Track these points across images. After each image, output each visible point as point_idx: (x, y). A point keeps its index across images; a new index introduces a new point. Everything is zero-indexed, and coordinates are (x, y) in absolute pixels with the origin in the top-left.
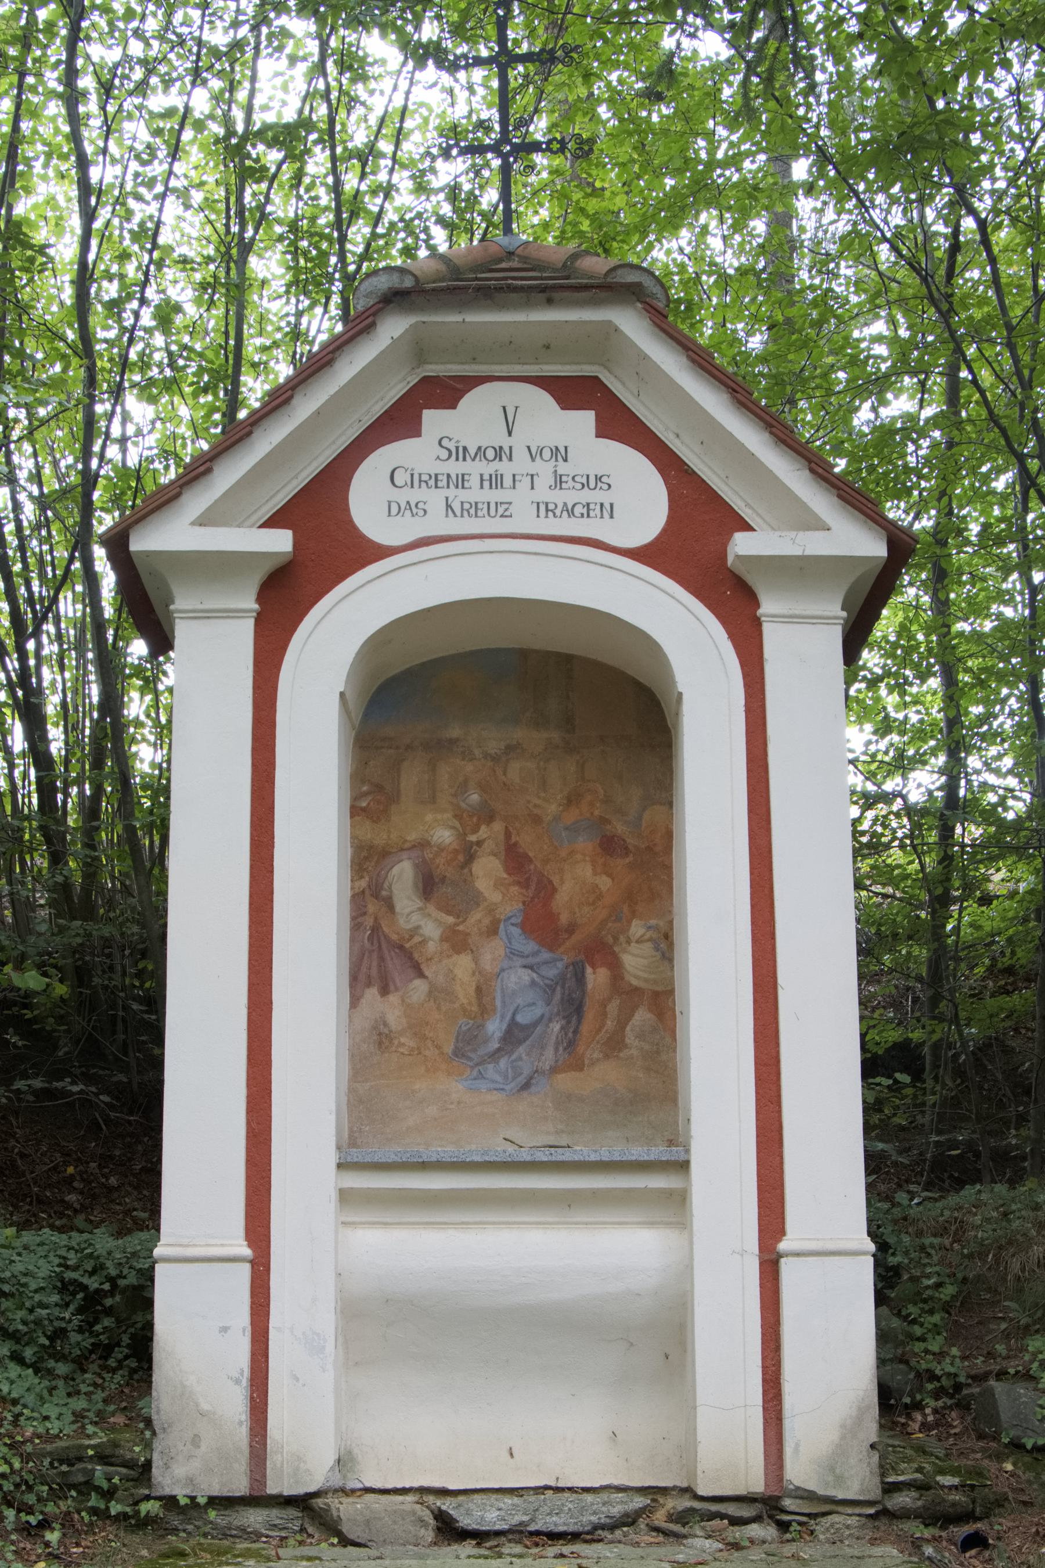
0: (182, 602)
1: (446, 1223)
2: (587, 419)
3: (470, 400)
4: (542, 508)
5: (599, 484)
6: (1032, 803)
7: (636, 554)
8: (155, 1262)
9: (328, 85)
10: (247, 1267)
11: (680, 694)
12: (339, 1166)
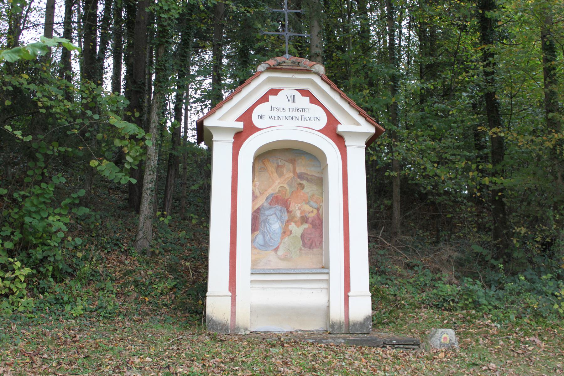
2: (308, 99)
7: (320, 131)
11: (327, 165)
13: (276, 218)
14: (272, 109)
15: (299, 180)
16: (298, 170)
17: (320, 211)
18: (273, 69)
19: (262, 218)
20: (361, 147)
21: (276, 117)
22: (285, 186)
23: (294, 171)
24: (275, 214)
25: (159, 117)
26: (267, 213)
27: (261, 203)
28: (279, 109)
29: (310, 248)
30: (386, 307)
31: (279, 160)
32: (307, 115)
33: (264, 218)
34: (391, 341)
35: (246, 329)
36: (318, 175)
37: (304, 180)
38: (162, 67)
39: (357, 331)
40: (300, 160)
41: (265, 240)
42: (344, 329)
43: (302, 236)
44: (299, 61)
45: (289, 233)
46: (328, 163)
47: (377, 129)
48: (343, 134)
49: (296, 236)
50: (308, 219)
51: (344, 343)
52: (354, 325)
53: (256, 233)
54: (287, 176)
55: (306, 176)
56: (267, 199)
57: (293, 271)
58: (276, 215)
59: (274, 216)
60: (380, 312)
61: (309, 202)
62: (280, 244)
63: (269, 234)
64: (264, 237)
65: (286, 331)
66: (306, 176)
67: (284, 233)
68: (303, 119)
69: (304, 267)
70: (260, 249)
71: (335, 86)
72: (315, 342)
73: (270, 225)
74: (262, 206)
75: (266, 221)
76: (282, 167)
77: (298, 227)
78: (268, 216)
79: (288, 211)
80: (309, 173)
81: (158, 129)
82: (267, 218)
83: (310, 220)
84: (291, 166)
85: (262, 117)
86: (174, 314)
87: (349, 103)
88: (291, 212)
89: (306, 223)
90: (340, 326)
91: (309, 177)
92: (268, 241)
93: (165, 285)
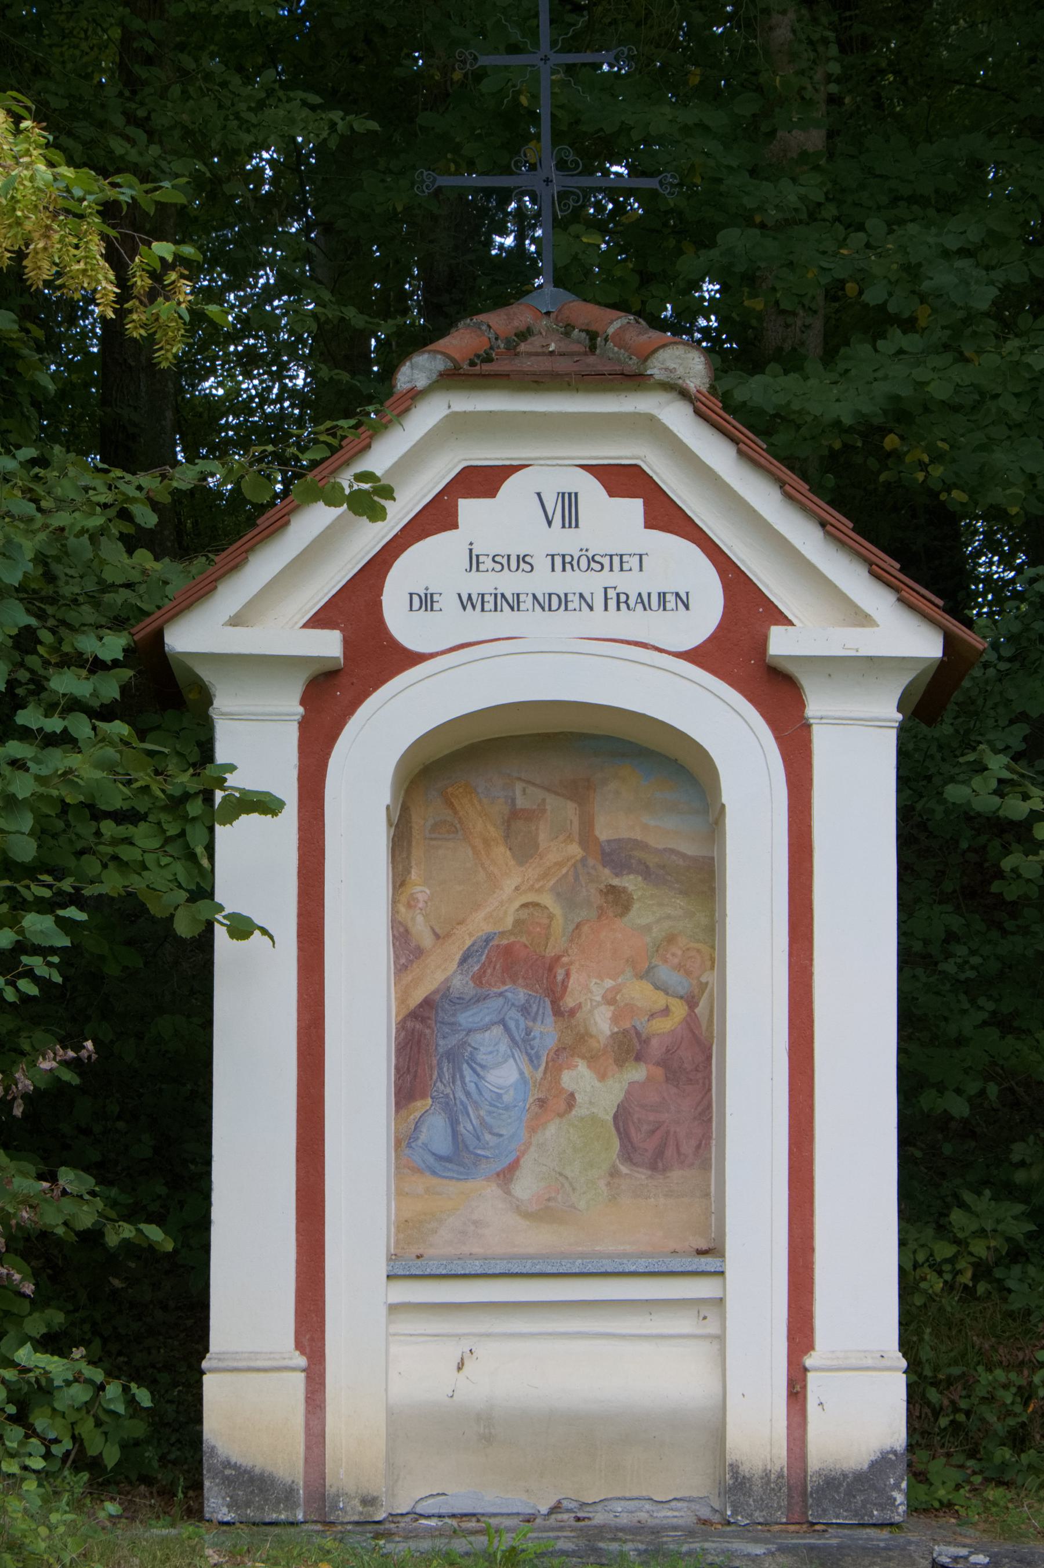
0: (223, 703)
1: (488, 1335)
2: (635, 507)
3: (510, 486)
4: (558, 561)
7: (691, 656)
10: (302, 1376)
11: (723, 806)
12: (388, 1276)
13: (506, 1040)
14: (474, 561)
15: (607, 871)
16: (604, 833)
17: (701, 1009)
22: (547, 900)
23: (587, 838)
24: (503, 1022)
28: (503, 562)
29: (653, 1167)
32: (630, 583)
33: (453, 1041)
36: (690, 849)
37: (631, 870)
43: (622, 1118)
45: (563, 1106)
46: (725, 799)
47: (950, 642)
48: (792, 669)
49: (593, 1118)
50: (646, 1042)
56: (464, 960)
59: (497, 1031)
61: (651, 969)
63: (477, 1106)
67: (542, 1103)
69: (628, 1248)
70: (434, 1173)
73: (479, 1069)
76: (529, 816)
77: (602, 1077)
79: (558, 1012)
80: (655, 841)
82: (464, 1044)
84: (570, 810)
85: (427, 601)
88: (572, 1013)
89: (638, 1058)
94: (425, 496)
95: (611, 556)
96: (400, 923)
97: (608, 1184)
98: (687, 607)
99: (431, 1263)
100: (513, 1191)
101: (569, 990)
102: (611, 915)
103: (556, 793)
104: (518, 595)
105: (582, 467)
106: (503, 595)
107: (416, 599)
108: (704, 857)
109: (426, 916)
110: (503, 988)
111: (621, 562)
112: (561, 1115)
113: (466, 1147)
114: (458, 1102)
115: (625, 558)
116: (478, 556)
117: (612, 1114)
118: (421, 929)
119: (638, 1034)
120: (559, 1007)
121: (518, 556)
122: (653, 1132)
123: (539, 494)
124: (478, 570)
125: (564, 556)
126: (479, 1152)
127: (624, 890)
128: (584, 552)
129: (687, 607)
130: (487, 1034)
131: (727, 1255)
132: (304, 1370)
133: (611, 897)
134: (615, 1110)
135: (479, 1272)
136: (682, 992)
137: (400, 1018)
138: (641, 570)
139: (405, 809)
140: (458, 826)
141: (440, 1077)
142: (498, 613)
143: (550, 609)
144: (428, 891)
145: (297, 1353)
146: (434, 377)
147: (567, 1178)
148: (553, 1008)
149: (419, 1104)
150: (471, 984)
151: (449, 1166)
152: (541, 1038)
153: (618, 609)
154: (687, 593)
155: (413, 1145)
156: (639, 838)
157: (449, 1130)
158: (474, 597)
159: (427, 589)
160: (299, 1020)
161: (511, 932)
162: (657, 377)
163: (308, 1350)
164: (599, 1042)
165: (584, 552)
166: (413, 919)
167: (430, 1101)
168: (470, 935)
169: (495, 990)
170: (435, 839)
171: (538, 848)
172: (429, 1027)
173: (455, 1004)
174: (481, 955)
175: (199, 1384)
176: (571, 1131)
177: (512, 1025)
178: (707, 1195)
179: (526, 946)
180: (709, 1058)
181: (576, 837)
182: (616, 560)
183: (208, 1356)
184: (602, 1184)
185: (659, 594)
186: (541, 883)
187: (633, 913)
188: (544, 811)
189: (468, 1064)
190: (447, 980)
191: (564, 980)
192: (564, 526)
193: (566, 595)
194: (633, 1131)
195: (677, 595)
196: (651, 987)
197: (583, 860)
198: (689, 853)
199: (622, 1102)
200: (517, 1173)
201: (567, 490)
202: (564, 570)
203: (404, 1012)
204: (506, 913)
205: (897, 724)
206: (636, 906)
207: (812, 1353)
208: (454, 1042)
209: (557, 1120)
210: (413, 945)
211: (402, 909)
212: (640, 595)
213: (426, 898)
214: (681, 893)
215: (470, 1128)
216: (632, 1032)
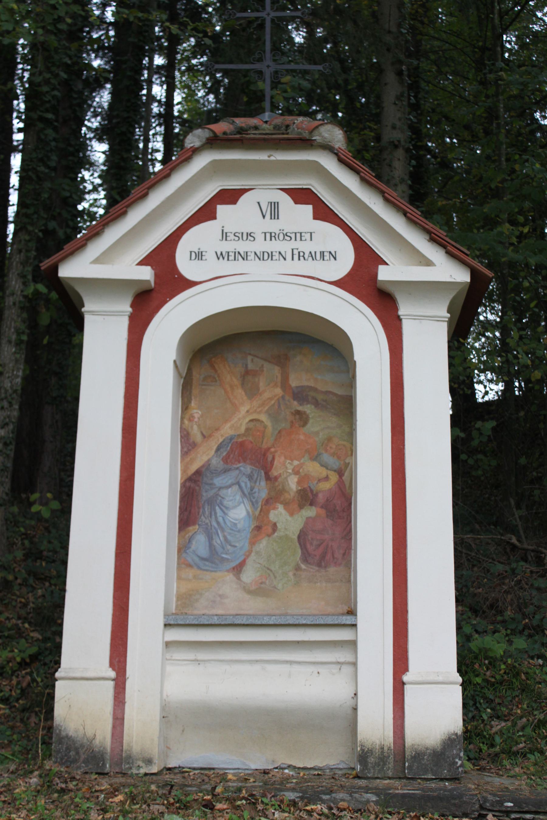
2: (308, 209)
3: (244, 199)
4: (268, 236)
5: (249, 238)
6: (495, 401)
7: (338, 283)
8: (56, 680)
9: (533, 551)
10: (112, 684)
11: (355, 362)
12: (165, 625)
13: (240, 493)
14: (225, 236)
15: (295, 403)
16: (294, 382)
17: (346, 477)
18: (222, 140)
19: (206, 495)
20: (436, 319)
21: (232, 254)
22: (263, 417)
23: (285, 384)
24: (238, 483)
25: (24, 284)
26: (218, 481)
27: (205, 458)
28: (239, 236)
29: (319, 565)
30: (530, 713)
31: (250, 358)
32: (306, 247)
33: (212, 493)
34: (501, 803)
35: (149, 761)
36: (340, 392)
37: (308, 402)
38: (30, 173)
39: (426, 773)
40: (299, 358)
41: (211, 546)
42: (391, 765)
43: (302, 537)
44: (288, 123)
45: (270, 530)
46: (356, 358)
47: (474, 274)
48: (391, 289)
49: (287, 536)
50: (315, 495)
51: (376, 803)
52: (418, 755)
53: (192, 529)
54: (267, 395)
55: (312, 394)
56: (218, 449)
57: (266, 621)
58: (240, 487)
59: (236, 488)
60: (514, 724)
61: (319, 455)
62: (248, 555)
63: (223, 530)
64: (210, 539)
65: (253, 767)
66: (312, 394)
67: (258, 528)
68: (296, 257)
69: (305, 611)
70: (199, 568)
71: (370, 176)
72: (302, 798)
73: (225, 509)
74: (207, 465)
75: (214, 502)
76: (255, 374)
77: (292, 514)
78: (220, 488)
79: (268, 478)
80: (320, 387)
81: (22, 308)
82: (217, 495)
83: (321, 498)
84: (276, 371)
85: (199, 255)
86: (22, 720)
87: (405, 214)
88: (276, 478)
89: (311, 504)
90: (383, 759)
91: (320, 397)
92: (219, 549)
93: (11, 655)
94: (200, 203)
95: (296, 233)
96: (185, 429)
97: (294, 574)
98: (335, 259)
99: (189, 617)
100: (242, 578)
101: (274, 466)
102: (297, 425)
103: (269, 362)
104: (247, 253)
105: (282, 189)
106: (239, 253)
107: (193, 254)
108: (347, 396)
109: (199, 426)
110: (239, 465)
111: (301, 236)
112: (269, 536)
113: (217, 553)
114: (213, 528)
115: (303, 234)
116: (226, 233)
117: (297, 535)
118: (196, 433)
119: (312, 491)
120: (269, 476)
121: (247, 233)
122: (319, 545)
123: (259, 203)
124: (226, 240)
125: (271, 233)
126: (224, 556)
127: (305, 413)
128: (281, 231)
129: (335, 259)
130: (230, 490)
131: (358, 614)
132: (113, 680)
133: (297, 417)
134: (298, 533)
135: (216, 623)
136: (336, 467)
137: (183, 481)
138: (311, 240)
139: (189, 370)
140: (217, 378)
141: (204, 513)
142: (236, 262)
143: (263, 260)
144: (200, 413)
145: (111, 669)
146: (204, 140)
147: (271, 571)
148: (265, 476)
149: (191, 528)
150: (222, 463)
151: (207, 563)
152: (259, 493)
153: (299, 259)
154: (335, 252)
155: (188, 551)
156: (313, 386)
157: (207, 543)
158: (224, 254)
159: (199, 249)
160: (121, 476)
161: (244, 435)
162: (318, 141)
163: (116, 668)
164: (290, 495)
165: (281, 231)
166: (192, 427)
167: (197, 527)
168: (222, 436)
169: (235, 466)
170: (205, 385)
171: (259, 390)
172: (198, 486)
173: (212, 473)
174: (227, 447)
175: (54, 686)
176: (275, 544)
177: (243, 485)
178: (349, 581)
179: (251, 442)
180: (350, 504)
181: (279, 384)
182: (298, 235)
183: (59, 670)
184: (291, 574)
185: (321, 252)
186: (260, 409)
187: (309, 426)
188: (263, 371)
189: (219, 506)
190: (209, 460)
191: (271, 461)
192: (271, 218)
193: (272, 252)
194: (308, 546)
195: (330, 253)
196: (319, 465)
197: (283, 397)
198: (339, 393)
199: (303, 528)
200: (244, 568)
201: (273, 201)
202: (271, 240)
203: (185, 477)
204: (241, 424)
205: (447, 319)
206: (311, 421)
207: (407, 673)
208: (212, 494)
209: (267, 538)
210: (191, 441)
211: (186, 422)
212: (310, 253)
213: (199, 416)
214: (335, 414)
215: (219, 542)
216: (308, 489)
